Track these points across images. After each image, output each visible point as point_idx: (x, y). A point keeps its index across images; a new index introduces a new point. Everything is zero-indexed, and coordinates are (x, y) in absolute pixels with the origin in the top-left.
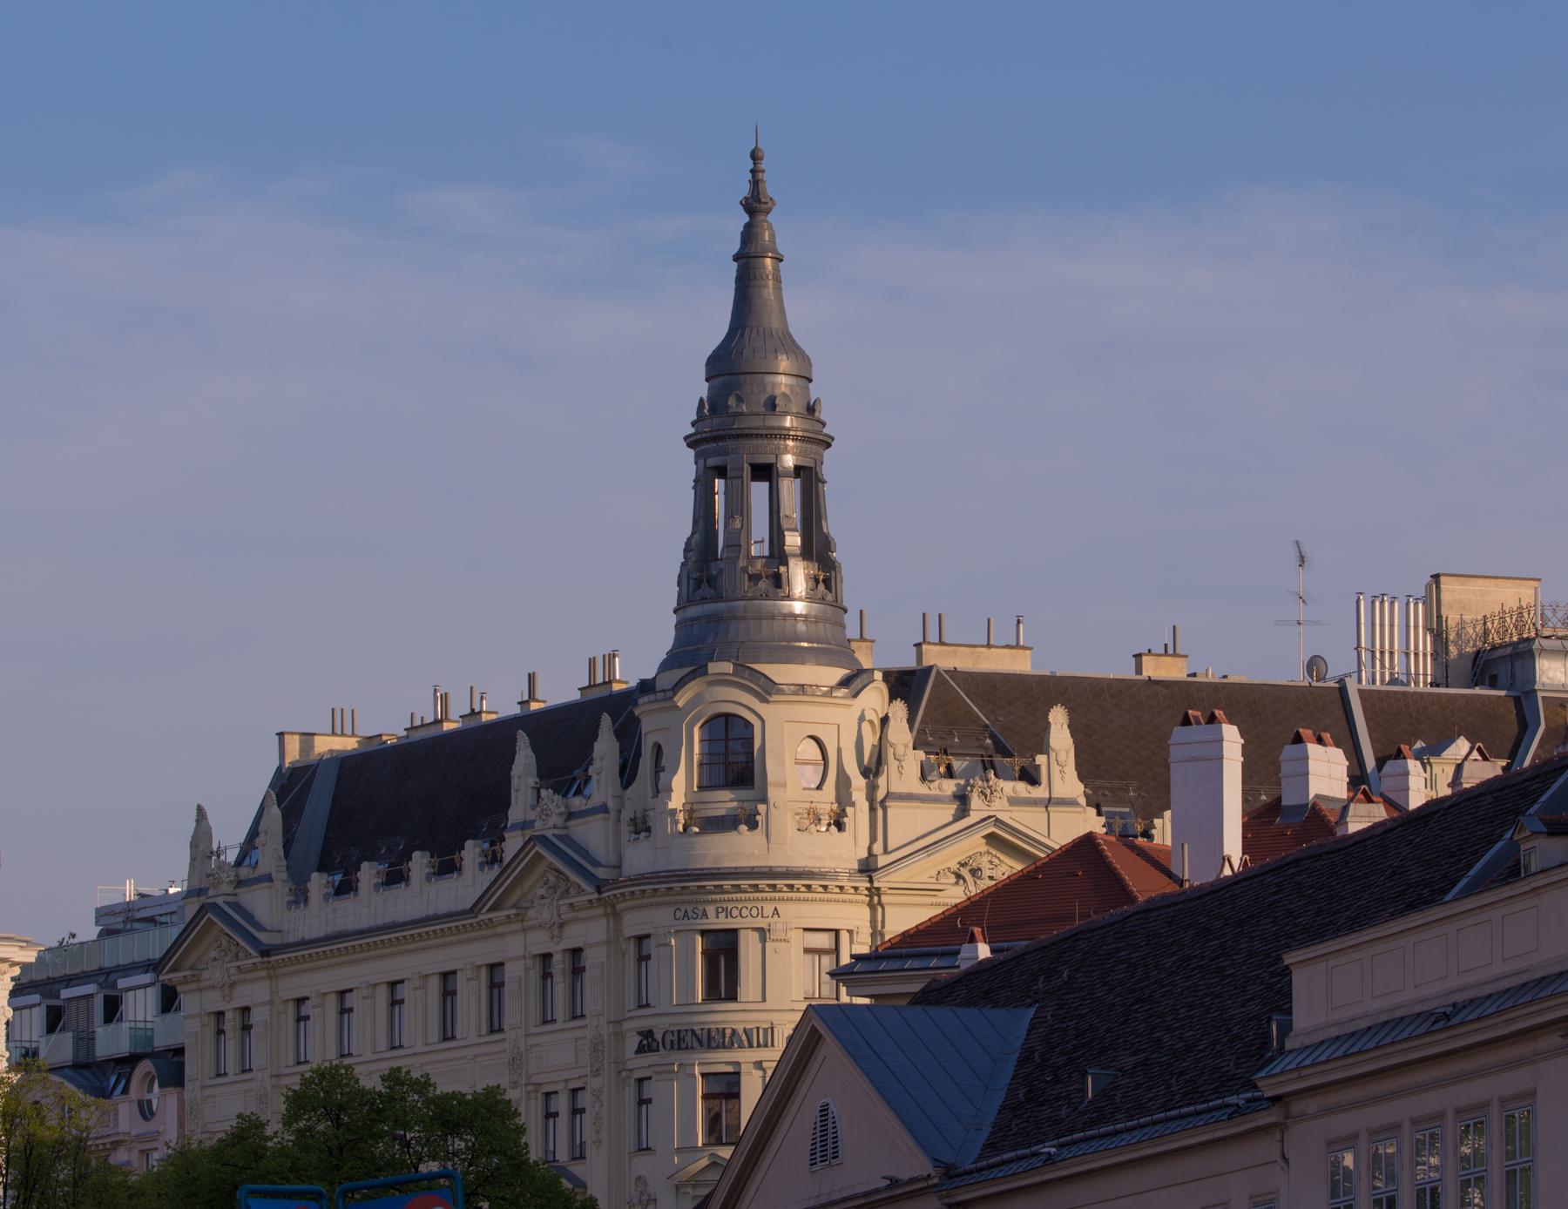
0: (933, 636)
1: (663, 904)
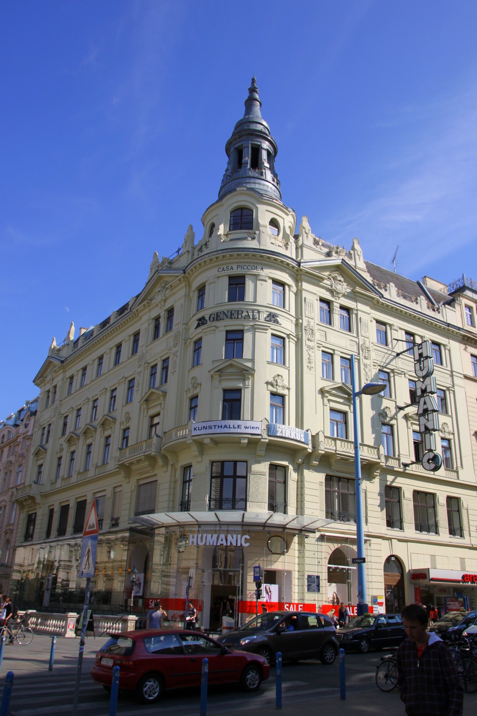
1: (211, 268)
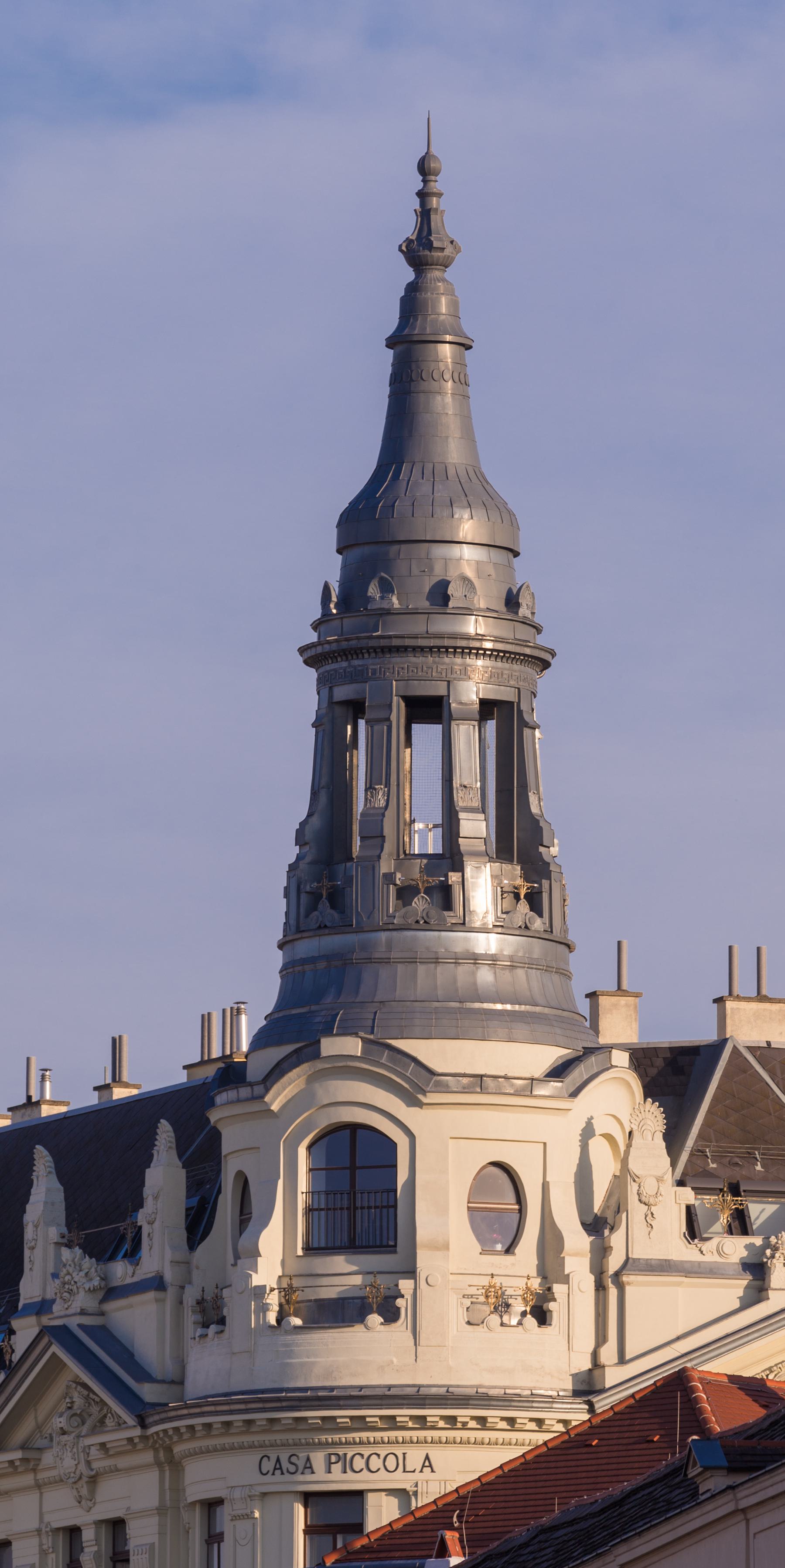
0: (744, 983)
